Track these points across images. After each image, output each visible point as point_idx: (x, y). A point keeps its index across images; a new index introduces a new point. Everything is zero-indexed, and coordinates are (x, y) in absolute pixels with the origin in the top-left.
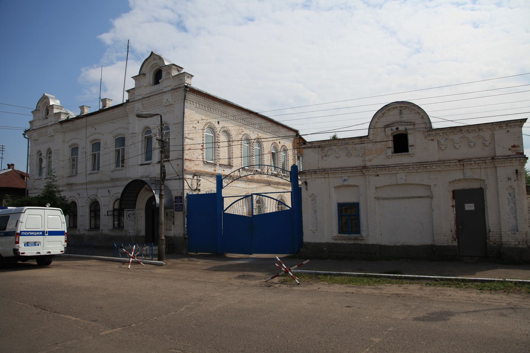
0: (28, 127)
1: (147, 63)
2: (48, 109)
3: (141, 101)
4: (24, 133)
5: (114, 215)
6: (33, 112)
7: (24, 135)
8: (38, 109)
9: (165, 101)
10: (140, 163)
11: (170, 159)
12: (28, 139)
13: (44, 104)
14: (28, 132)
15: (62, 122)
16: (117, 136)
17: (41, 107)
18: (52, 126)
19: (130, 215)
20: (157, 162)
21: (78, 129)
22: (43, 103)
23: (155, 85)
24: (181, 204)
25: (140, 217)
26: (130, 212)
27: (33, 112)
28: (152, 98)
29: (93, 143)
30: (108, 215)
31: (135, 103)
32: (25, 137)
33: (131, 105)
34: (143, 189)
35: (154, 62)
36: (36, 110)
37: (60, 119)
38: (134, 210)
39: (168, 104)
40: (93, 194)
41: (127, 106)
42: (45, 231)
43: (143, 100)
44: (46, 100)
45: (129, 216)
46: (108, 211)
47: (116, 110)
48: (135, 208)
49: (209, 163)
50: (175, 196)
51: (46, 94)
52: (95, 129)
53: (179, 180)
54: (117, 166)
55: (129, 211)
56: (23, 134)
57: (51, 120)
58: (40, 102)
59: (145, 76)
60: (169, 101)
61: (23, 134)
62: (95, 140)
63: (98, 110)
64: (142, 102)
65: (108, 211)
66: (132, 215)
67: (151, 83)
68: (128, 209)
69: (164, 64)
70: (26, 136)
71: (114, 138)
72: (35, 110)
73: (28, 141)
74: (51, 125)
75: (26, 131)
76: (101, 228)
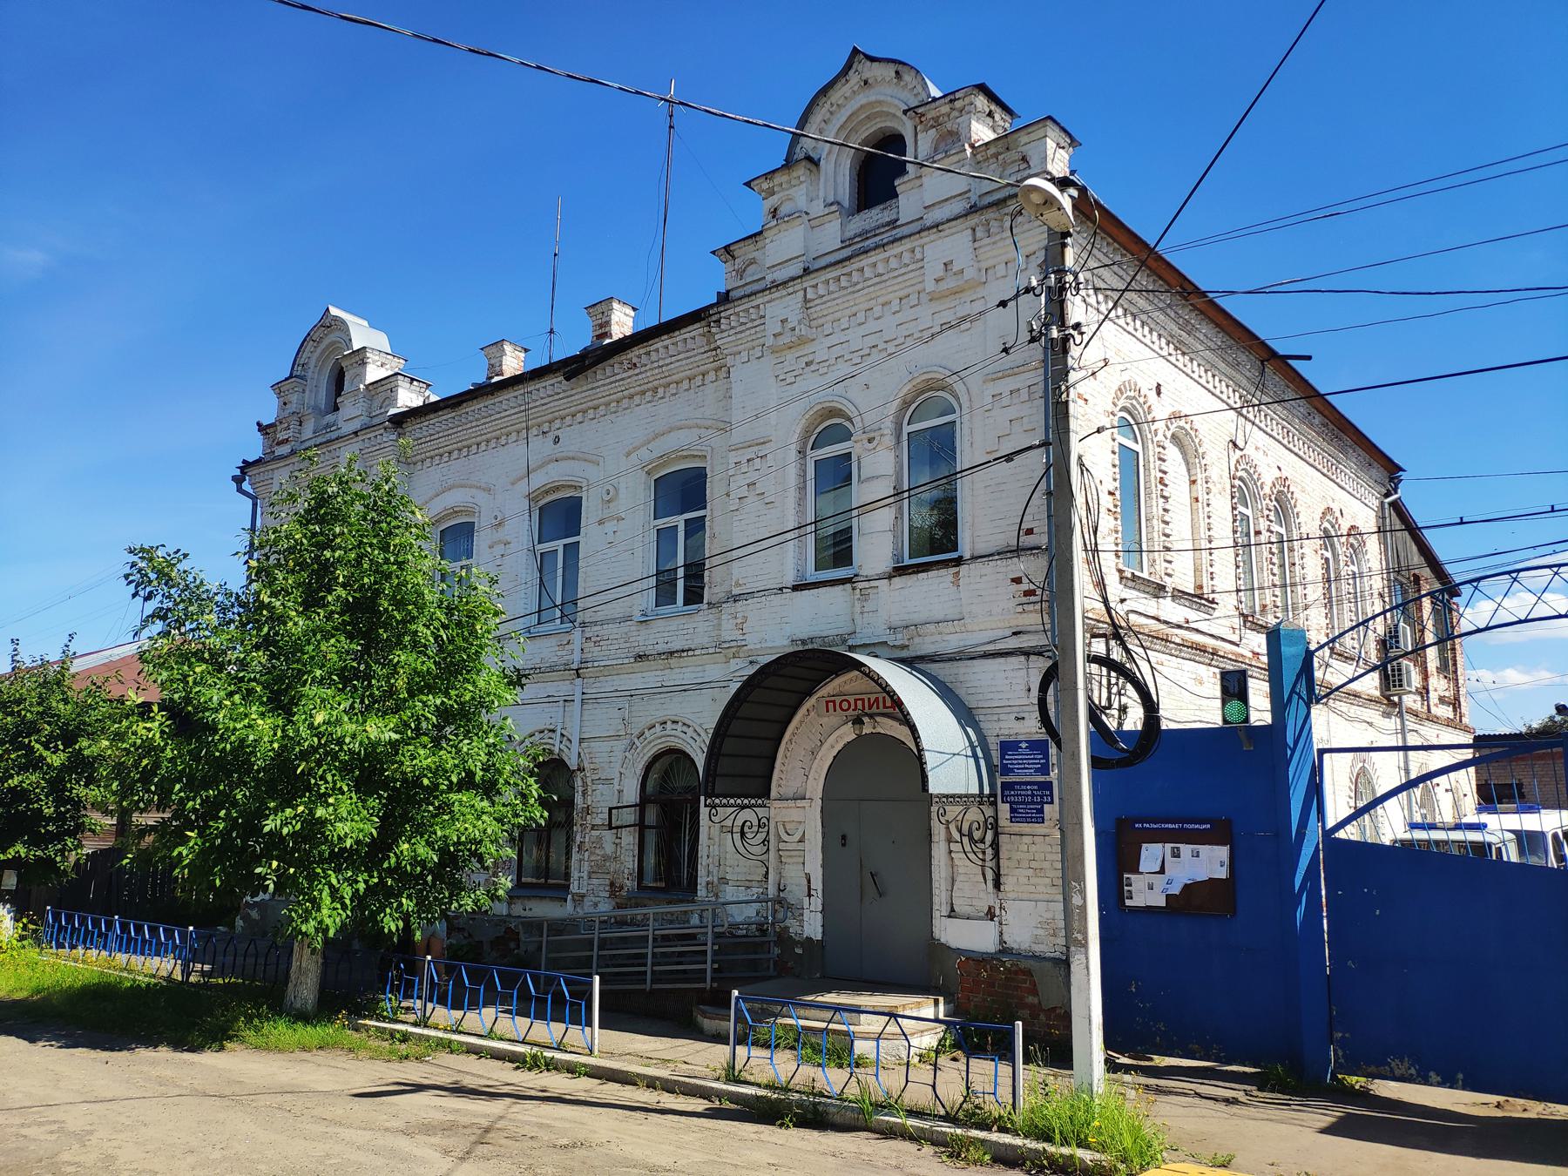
0: (254, 448)
1: (827, 106)
2: (342, 368)
3: (798, 287)
4: (238, 472)
5: (641, 826)
6: (277, 387)
7: (239, 480)
8: (298, 372)
9: (934, 269)
10: (790, 580)
11: (965, 549)
12: (254, 498)
13: (324, 351)
14: (252, 471)
15: (400, 421)
16: (663, 465)
17: (312, 365)
18: (361, 438)
19: (746, 829)
20: (889, 569)
21: (514, 434)
22: (323, 346)
23: (859, 210)
24: (1041, 779)
25: (797, 837)
26: (747, 815)
27: (277, 387)
28: (813, 282)
29: (542, 503)
30: (611, 828)
31: (766, 299)
32: (240, 490)
33: (747, 311)
34: (810, 702)
35: (862, 99)
36: (291, 376)
37: (395, 406)
38: (760, 806)
39: (950, 283)
40: (542, 728)
41: (723, 321)
42: (1543, 834)
43: (808, 282)
44: (332, 337)
45: (743, 834)
46: (610, 809)
47: (659, 345)
48: (765, 793)
49: (1141, 581)
50: (1002, 738)
51: (334, 311)
52: (557, 440)
53: (1022, 658)
54: (664, 592)
55: (743, 807)
56: (234, 478)
57: (351, 412)
58: (310, 346)
59: (813, 168)
60: (956, 267)
61: (234, 478)
62: (557, 489)
63: (546, 362)
64: (805, 290)
65: (610, 809)
66: (755, 829)
67: (846, 204)
68: (739, 801)
69: (929, 96)
70: (246, 486)
71: (648, 473)
72: (286, 379)
73: (255, 505)
74: (356, 433)
75: (246, 466)
76: (574, 888)
